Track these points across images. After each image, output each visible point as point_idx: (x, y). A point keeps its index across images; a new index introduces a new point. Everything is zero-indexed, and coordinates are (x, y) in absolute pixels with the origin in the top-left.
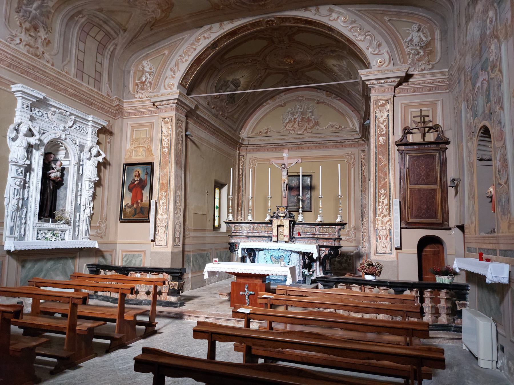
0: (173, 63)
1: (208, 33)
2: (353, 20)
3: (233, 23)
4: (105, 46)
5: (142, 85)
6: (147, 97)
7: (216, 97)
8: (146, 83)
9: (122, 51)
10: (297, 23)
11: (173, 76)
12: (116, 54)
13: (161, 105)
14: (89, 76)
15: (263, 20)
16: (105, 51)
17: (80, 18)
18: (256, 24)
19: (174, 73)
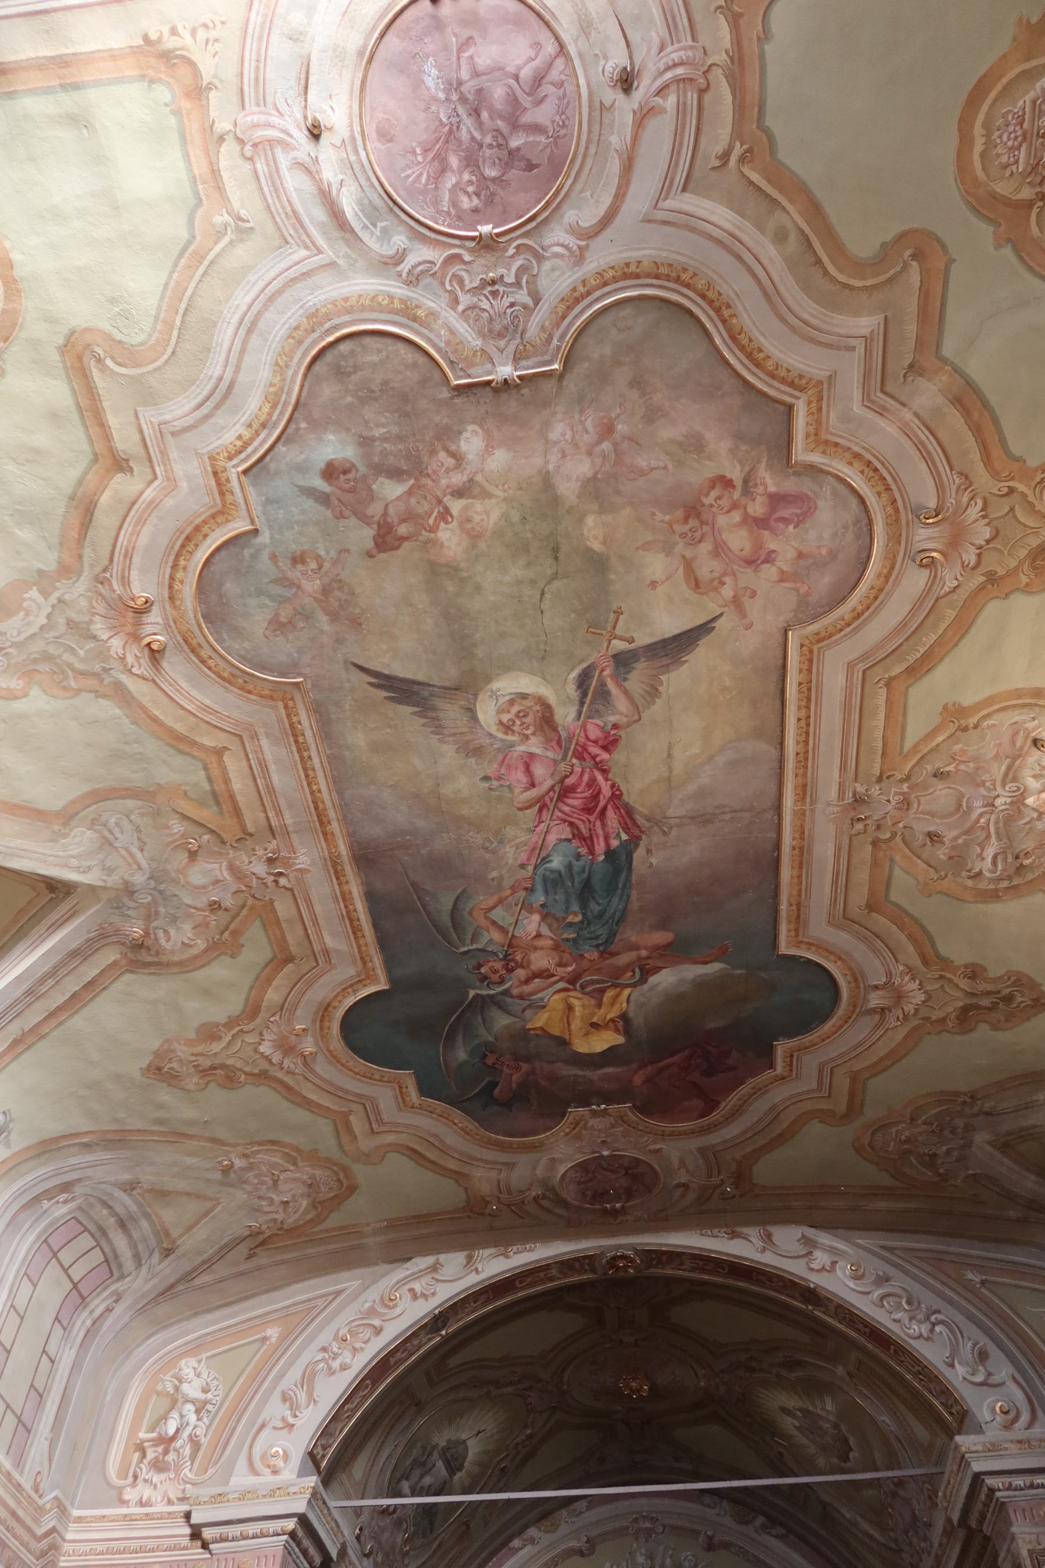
0: (295, 1373)
1: (427, 1279)
2: (881, 1273)
3: (507, 1257)
4: (83, 1299)
5: (160, 1449)
6: (170, 1502)
7: (385, 1511)
8: (178, 1444)
9: (126, 1319)
10: (703, 1270)
11: (291, 1420)
12: (104, 1329)
13: (226, 1540)
14: (8, 1406)
15: (603, 1254)
16: (79, 1316)
17: (58, 1202)
18: (577, 1265)
19: (295, 1409)
